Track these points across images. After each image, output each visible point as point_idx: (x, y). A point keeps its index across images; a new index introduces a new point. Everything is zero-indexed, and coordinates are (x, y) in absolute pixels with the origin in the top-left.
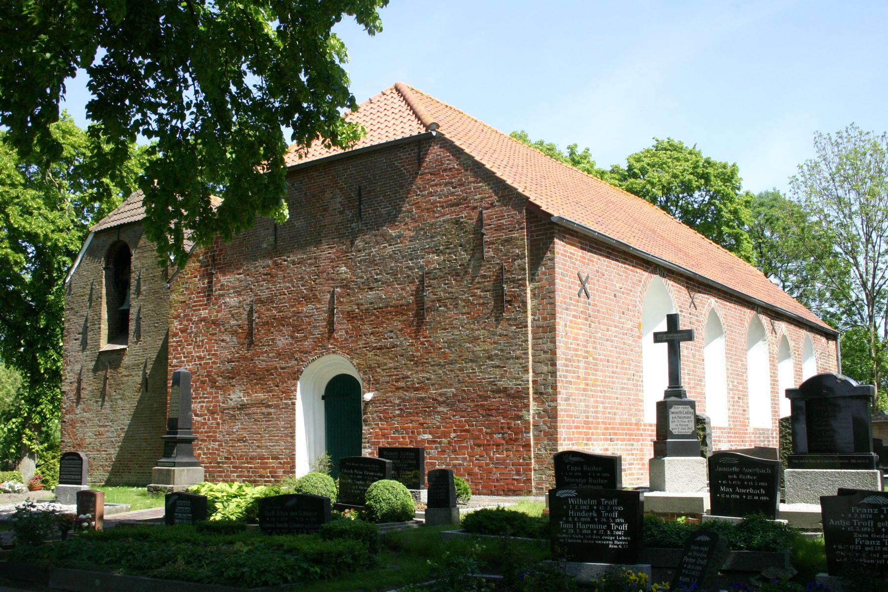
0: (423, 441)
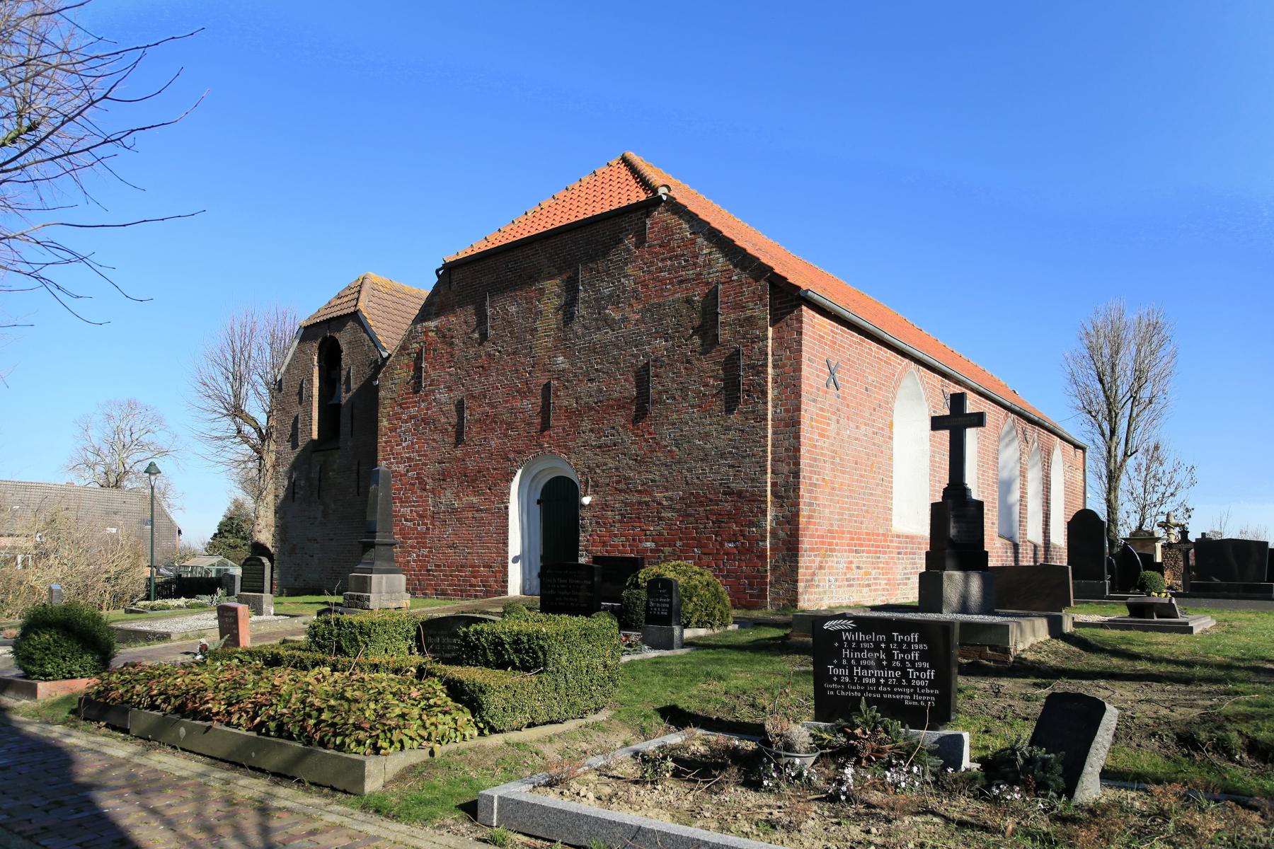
0: (646, 549)
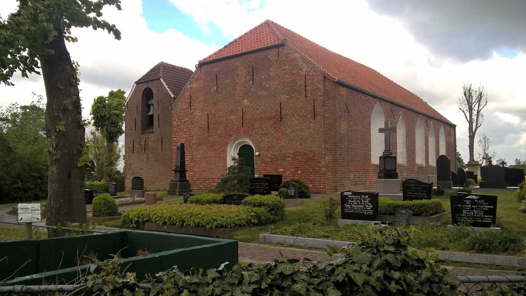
0: (280, 172)
